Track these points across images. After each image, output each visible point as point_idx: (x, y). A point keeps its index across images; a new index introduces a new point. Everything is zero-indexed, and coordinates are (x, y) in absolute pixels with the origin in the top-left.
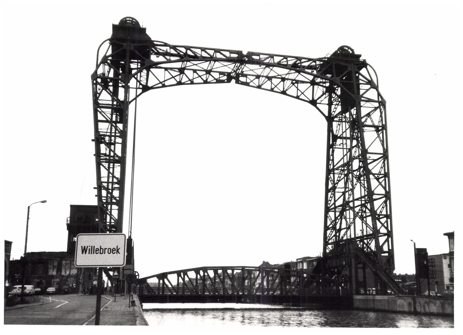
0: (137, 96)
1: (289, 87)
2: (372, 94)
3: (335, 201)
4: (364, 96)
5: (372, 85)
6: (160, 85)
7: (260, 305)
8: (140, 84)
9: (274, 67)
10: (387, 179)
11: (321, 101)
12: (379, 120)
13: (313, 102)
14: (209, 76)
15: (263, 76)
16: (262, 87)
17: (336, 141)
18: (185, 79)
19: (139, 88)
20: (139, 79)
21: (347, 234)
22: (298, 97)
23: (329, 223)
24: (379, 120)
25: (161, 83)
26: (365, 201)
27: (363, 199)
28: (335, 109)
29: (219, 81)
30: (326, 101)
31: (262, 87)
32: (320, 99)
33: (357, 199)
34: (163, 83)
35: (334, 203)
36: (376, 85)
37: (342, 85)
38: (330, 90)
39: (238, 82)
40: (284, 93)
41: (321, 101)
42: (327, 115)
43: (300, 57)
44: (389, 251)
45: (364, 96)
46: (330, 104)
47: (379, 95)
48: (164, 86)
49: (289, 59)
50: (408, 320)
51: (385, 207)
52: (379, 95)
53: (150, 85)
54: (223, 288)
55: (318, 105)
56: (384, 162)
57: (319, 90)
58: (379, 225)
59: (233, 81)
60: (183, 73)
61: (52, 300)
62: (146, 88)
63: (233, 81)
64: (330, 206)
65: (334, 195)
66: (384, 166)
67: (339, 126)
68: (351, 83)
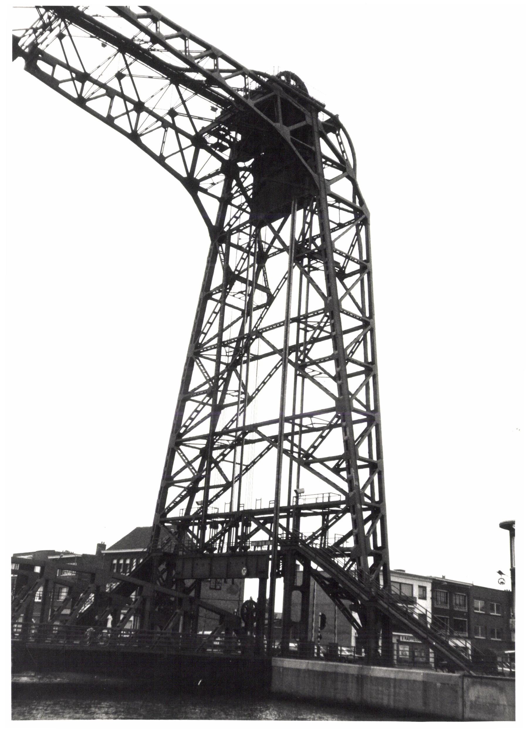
1: (147, 129)
3: (222, 330)
4: (309, 312)
10: (366, 276)
11: (213, 184)
17: (232, 285)
21: (237, 419)
22: (161, 160)
23: (178, 463)
26: (301, 426)
28: (195, 414)
30: (218, 191)
31: (88, 104)
32: (210, 181)
33: (287, 420)
35: (219, 335)
36: (351, 167)
37: (176, 590)
42: (214, 222)
43: (186, 31)
45: (309, 312)
47: (356, 191)
50: (404, 665)
51: (357, 242)
52: (356, 191)
55: (200, 194)
56: (358, 234)
58: (341, 291)
63: (21, 61)
64: (205, 341)
65: (222, 311)
66: (359, 240)
67: (242, 261)
68: (310, 150)
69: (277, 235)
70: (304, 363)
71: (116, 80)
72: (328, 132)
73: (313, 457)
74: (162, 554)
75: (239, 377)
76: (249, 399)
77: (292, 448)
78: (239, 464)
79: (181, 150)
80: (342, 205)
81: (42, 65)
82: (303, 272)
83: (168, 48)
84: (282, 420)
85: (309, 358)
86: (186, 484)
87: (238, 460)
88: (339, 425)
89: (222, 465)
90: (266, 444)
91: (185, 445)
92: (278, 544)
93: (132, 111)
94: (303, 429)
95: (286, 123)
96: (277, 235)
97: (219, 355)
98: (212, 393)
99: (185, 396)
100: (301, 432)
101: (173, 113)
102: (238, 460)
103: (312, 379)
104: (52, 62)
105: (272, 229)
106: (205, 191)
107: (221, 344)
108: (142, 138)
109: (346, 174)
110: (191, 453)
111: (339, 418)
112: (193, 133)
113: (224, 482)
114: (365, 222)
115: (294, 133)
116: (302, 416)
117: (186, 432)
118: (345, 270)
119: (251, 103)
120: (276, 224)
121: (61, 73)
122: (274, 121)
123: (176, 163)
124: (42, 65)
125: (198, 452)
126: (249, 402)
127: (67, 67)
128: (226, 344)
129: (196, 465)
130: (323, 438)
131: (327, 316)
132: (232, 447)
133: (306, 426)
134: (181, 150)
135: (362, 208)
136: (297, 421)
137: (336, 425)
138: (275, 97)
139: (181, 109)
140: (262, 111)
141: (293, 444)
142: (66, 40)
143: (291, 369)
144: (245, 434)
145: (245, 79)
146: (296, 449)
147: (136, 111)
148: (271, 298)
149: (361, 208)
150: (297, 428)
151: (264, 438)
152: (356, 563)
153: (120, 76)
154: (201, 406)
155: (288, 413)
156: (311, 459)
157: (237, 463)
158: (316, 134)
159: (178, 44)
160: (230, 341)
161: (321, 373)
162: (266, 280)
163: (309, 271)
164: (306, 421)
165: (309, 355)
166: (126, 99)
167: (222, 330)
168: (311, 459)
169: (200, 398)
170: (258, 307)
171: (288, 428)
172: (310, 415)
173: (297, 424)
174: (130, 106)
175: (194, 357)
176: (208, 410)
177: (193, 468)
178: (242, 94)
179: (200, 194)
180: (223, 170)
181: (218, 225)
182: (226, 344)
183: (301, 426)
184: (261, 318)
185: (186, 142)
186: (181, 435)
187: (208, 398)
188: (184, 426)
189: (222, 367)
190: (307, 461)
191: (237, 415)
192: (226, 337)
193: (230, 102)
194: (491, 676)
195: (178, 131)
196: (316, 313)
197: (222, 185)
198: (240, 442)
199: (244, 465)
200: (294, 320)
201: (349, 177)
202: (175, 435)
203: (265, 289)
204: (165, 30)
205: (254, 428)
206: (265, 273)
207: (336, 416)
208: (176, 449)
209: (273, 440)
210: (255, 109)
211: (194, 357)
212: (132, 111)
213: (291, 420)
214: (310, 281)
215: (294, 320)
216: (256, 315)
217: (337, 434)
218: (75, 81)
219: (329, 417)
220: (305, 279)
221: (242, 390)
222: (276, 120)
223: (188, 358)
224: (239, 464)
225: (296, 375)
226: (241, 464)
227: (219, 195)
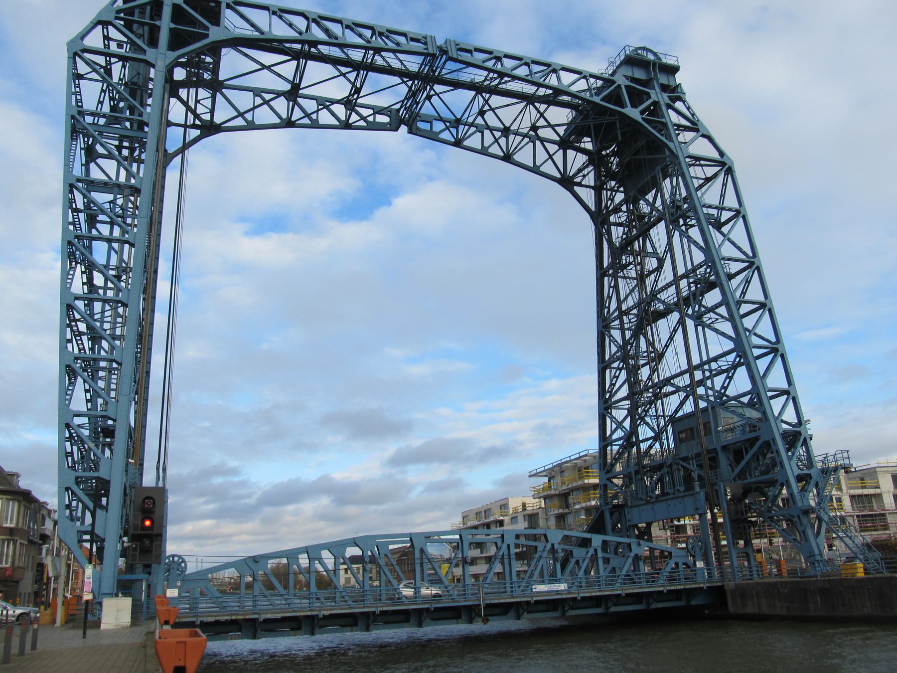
0: (186, 146)
2: (701, 147)
5: (694, 126)
6: (240, 122)
7: (509, 629)
8: (197, 116)
9: (551, 107)
12: (658, 231)
13: (567, 182)
14: (280, 117)
15: (516, 133)
16: (466, 143)
18: (297, 114)
19: (194, 126)
20: (192, 103)
22: (535, 170)
24: (658, 231)
25: (241, 115)
26: (710, 371)
27: (701, 391)
29: (373, 126)
30: (590, 180)
31: (466, 143)
33: (697, 367)
34: (249, 116)
35: (619, 307)
38: (595, 159)
39: (413, 131)
40: (507, 158)
41: (584, 176)
42: (592, 206)
44: (130, 535)
46: (598, 189)
48: (251, 126)
49: (536, 68)
53: (218, 120)
54: (707, 570)
55: (576, 188)
57: (576, 160)
59: (404, 129)
60: (296, 103)
61: (563, 550)
62: (210, 129)
63: (404, 129)
69: (652, 205)
70: (699, 314)
71: (480, 118)
72: (674, 103)
73: (727, 396)
74: (611, 506)
75: (646, 337)
76: (661, 356)
77: (706, 391)
78: (661, 416)
79: (551, 157)
80: (702, 162)
81: (421, 125)
82: (682, 234)
83: (515, 78)
84: (691, 370)
85: (704, 307)
86: (620, 442)
87: (661, 413)
88: (742, 364)
89: (647, 419)
90: (682, 395)
91: (615, 408)
92: (179, 584)
93: (500, 137)
94: (713, 373)
95: (634, 105)
96: (652, 205)
97: (622, 323)
98: (624, 358)
99: (603, 365)
100: (711, 377)
101: (534, 128)
102: (661, 413)
103: (709, 326)
104: (429, 120)
105: (647, 201)
106: (579, 184)
107: (622, 313)
108: (515, 157)
109: (700, 134)
110: (620, 414)
111: (740, 357)
112: (558, 139)
113: (652, 434)
114: (730, 171)
115: (642, 113)
116: (709, 361)
117: (610, 397)
118: (720, 219)
119: (597, 99)
120: (650, 197)
121: (438, 126)
122: (623, 107)
123: (549, 168)
124: (421, 125)
125: (626, 412)
126: (660, 360)
127: (441, 119)
128: (627, 312)
129: (627, 424)
130: (731, 378)
131: (709, 266)
132: (651, 402)
133: (715, 370)
134: (551, 157)
135: (725, 159)
136: (706, 367)
137: (739, 364)
138: (619, 86)
139: (542, 122)
140: (610, 104)
141: (707, 388)
142: (435, 99)
143: (690, 323)
144: (661, 388)
145: (587, 80)
146: (710, 392)
147: (505, 137)
148: (661, 261)
149: (722, 160)
150: (707, 374)
151: (678, 390)
152: (785, 488)
153: (482, 113)
154: (618, 372)
155: (696, 361)
156: (725, 398)
157: (660, 416)
158: (664, 108)
159: (522, 71)
160: (630, 309)
161: (717, 320)
162: (653, 247)
163: (687, 230)
164: (714, 365)
165: (704, 303)
166: (491, 129)
167: (619, 302)
168: (725, 398)
169: (615, 365)
170: (651, 273)
171: (698, 375)
172: (715, 359)
173: (707, 370)
174: (498, 134)
175: (603, 330)
176: (623, 375)
177: (624, 427)
178: (587, 95)
179: (576, 188)
180: (591, 162)
181: (597, 211)
182: (627, 312)
183: (710, 371)
184: (656, 281)
185: (552, 148)
186: (606, 401)
187: (622, 364)
188: (608, 392)
189: (628, 334)
190: (721, 402)
191: (650, 375)
192: (624, 307)
193: (579, 105)
194: (806, 579)
195: (543, 141)
196: (700, 266)
197: (592, 175)
198: (657, 397)
199: (667, 416)
200: (683, 277)
201: (704, 136)
202: (602, 402)
203: (655, 254)
204: (508, 63)
205: (667, 381)
206: (651, 241)
207: (738, 356)
208: (606, 414)
209: (688, 389)
210: (142, 532)
211: (603, 330)
212: (500, 137)
213: (699, 367)
214: (690, 239)
215: (683, 277)
216: (649, 281)
217: (742, 371)
218: (451, 129)
219: (731, 357)
220: (685, 240)
221: (652, 350)
222: (623, 106)
223: (598, 333)
224: (661, 416)
225: (696, 327)
226: (664, 416)
227: (592, 184)
